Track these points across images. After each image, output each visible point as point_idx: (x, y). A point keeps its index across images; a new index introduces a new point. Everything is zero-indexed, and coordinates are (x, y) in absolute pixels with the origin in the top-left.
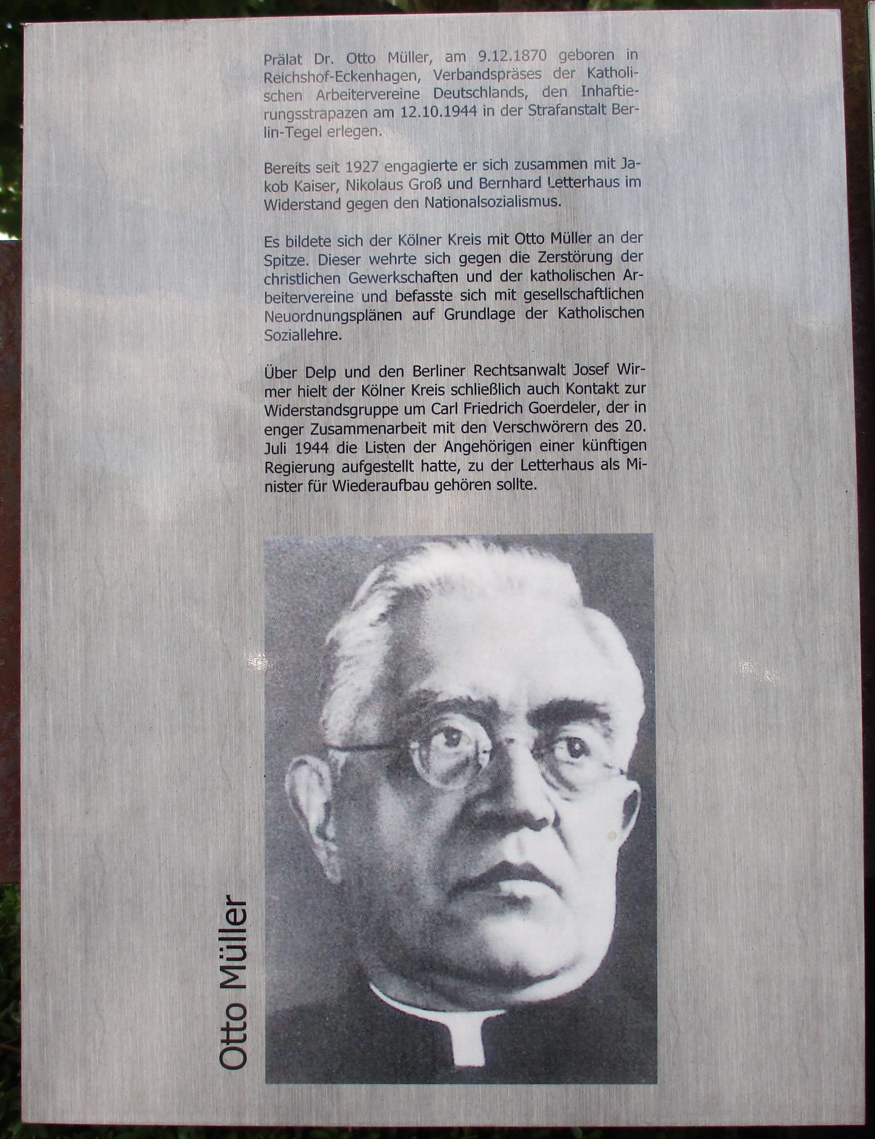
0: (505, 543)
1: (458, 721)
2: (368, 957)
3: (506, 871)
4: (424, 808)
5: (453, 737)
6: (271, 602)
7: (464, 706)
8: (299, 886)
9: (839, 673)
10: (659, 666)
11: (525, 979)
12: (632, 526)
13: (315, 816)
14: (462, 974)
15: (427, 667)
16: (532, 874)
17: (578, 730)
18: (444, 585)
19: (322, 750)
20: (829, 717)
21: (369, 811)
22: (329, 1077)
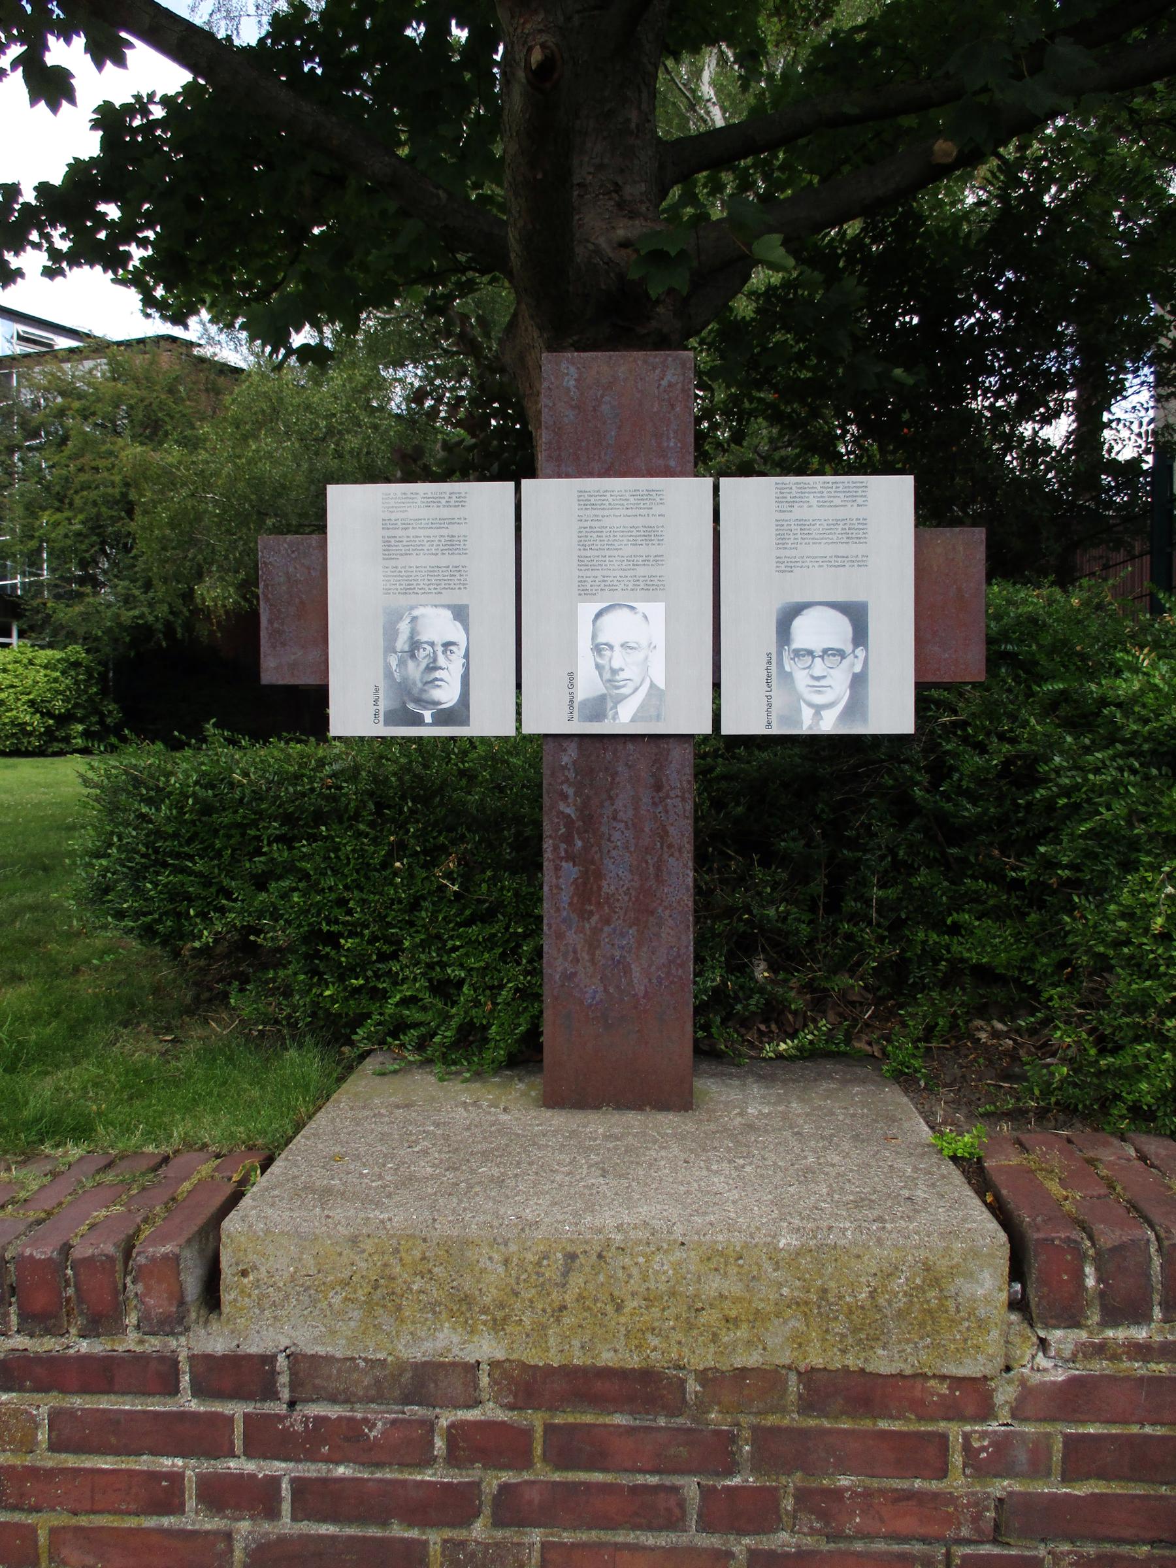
0: (436, 606)
1: (426, 646)
2: (406, 698)
3: (436, 679)
4: (418, 665)
5: (424, 649)
6: (241, 485)
7: (426, 643)
8: (1064, 873)
9: (438, 782)
10: (471, 632)
11: (440, 703)
12: (464, 602)
13: (394, 667)
14: (427, 702)
15: (418, 634)
16: (442, 680)
17: (451, 648)
18: (423, 615)
19: (395, 652)
20: (654, 369)
21: (406, 665)
22: (397, 725)
